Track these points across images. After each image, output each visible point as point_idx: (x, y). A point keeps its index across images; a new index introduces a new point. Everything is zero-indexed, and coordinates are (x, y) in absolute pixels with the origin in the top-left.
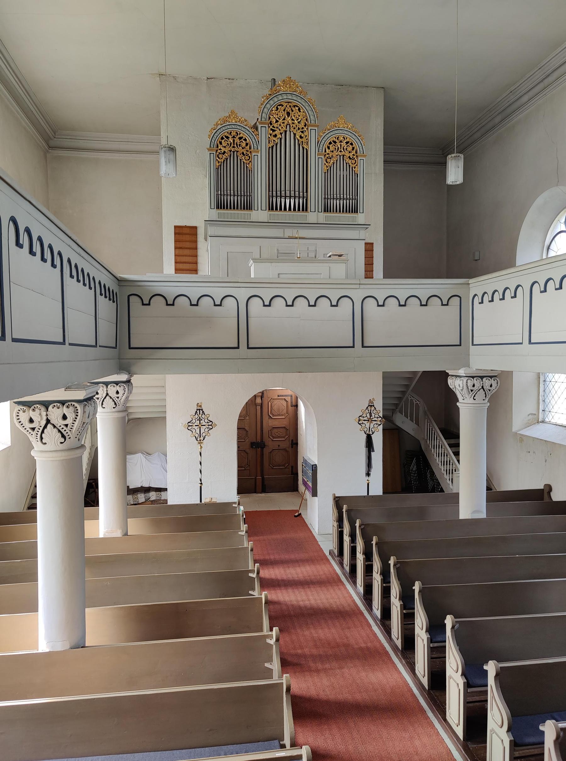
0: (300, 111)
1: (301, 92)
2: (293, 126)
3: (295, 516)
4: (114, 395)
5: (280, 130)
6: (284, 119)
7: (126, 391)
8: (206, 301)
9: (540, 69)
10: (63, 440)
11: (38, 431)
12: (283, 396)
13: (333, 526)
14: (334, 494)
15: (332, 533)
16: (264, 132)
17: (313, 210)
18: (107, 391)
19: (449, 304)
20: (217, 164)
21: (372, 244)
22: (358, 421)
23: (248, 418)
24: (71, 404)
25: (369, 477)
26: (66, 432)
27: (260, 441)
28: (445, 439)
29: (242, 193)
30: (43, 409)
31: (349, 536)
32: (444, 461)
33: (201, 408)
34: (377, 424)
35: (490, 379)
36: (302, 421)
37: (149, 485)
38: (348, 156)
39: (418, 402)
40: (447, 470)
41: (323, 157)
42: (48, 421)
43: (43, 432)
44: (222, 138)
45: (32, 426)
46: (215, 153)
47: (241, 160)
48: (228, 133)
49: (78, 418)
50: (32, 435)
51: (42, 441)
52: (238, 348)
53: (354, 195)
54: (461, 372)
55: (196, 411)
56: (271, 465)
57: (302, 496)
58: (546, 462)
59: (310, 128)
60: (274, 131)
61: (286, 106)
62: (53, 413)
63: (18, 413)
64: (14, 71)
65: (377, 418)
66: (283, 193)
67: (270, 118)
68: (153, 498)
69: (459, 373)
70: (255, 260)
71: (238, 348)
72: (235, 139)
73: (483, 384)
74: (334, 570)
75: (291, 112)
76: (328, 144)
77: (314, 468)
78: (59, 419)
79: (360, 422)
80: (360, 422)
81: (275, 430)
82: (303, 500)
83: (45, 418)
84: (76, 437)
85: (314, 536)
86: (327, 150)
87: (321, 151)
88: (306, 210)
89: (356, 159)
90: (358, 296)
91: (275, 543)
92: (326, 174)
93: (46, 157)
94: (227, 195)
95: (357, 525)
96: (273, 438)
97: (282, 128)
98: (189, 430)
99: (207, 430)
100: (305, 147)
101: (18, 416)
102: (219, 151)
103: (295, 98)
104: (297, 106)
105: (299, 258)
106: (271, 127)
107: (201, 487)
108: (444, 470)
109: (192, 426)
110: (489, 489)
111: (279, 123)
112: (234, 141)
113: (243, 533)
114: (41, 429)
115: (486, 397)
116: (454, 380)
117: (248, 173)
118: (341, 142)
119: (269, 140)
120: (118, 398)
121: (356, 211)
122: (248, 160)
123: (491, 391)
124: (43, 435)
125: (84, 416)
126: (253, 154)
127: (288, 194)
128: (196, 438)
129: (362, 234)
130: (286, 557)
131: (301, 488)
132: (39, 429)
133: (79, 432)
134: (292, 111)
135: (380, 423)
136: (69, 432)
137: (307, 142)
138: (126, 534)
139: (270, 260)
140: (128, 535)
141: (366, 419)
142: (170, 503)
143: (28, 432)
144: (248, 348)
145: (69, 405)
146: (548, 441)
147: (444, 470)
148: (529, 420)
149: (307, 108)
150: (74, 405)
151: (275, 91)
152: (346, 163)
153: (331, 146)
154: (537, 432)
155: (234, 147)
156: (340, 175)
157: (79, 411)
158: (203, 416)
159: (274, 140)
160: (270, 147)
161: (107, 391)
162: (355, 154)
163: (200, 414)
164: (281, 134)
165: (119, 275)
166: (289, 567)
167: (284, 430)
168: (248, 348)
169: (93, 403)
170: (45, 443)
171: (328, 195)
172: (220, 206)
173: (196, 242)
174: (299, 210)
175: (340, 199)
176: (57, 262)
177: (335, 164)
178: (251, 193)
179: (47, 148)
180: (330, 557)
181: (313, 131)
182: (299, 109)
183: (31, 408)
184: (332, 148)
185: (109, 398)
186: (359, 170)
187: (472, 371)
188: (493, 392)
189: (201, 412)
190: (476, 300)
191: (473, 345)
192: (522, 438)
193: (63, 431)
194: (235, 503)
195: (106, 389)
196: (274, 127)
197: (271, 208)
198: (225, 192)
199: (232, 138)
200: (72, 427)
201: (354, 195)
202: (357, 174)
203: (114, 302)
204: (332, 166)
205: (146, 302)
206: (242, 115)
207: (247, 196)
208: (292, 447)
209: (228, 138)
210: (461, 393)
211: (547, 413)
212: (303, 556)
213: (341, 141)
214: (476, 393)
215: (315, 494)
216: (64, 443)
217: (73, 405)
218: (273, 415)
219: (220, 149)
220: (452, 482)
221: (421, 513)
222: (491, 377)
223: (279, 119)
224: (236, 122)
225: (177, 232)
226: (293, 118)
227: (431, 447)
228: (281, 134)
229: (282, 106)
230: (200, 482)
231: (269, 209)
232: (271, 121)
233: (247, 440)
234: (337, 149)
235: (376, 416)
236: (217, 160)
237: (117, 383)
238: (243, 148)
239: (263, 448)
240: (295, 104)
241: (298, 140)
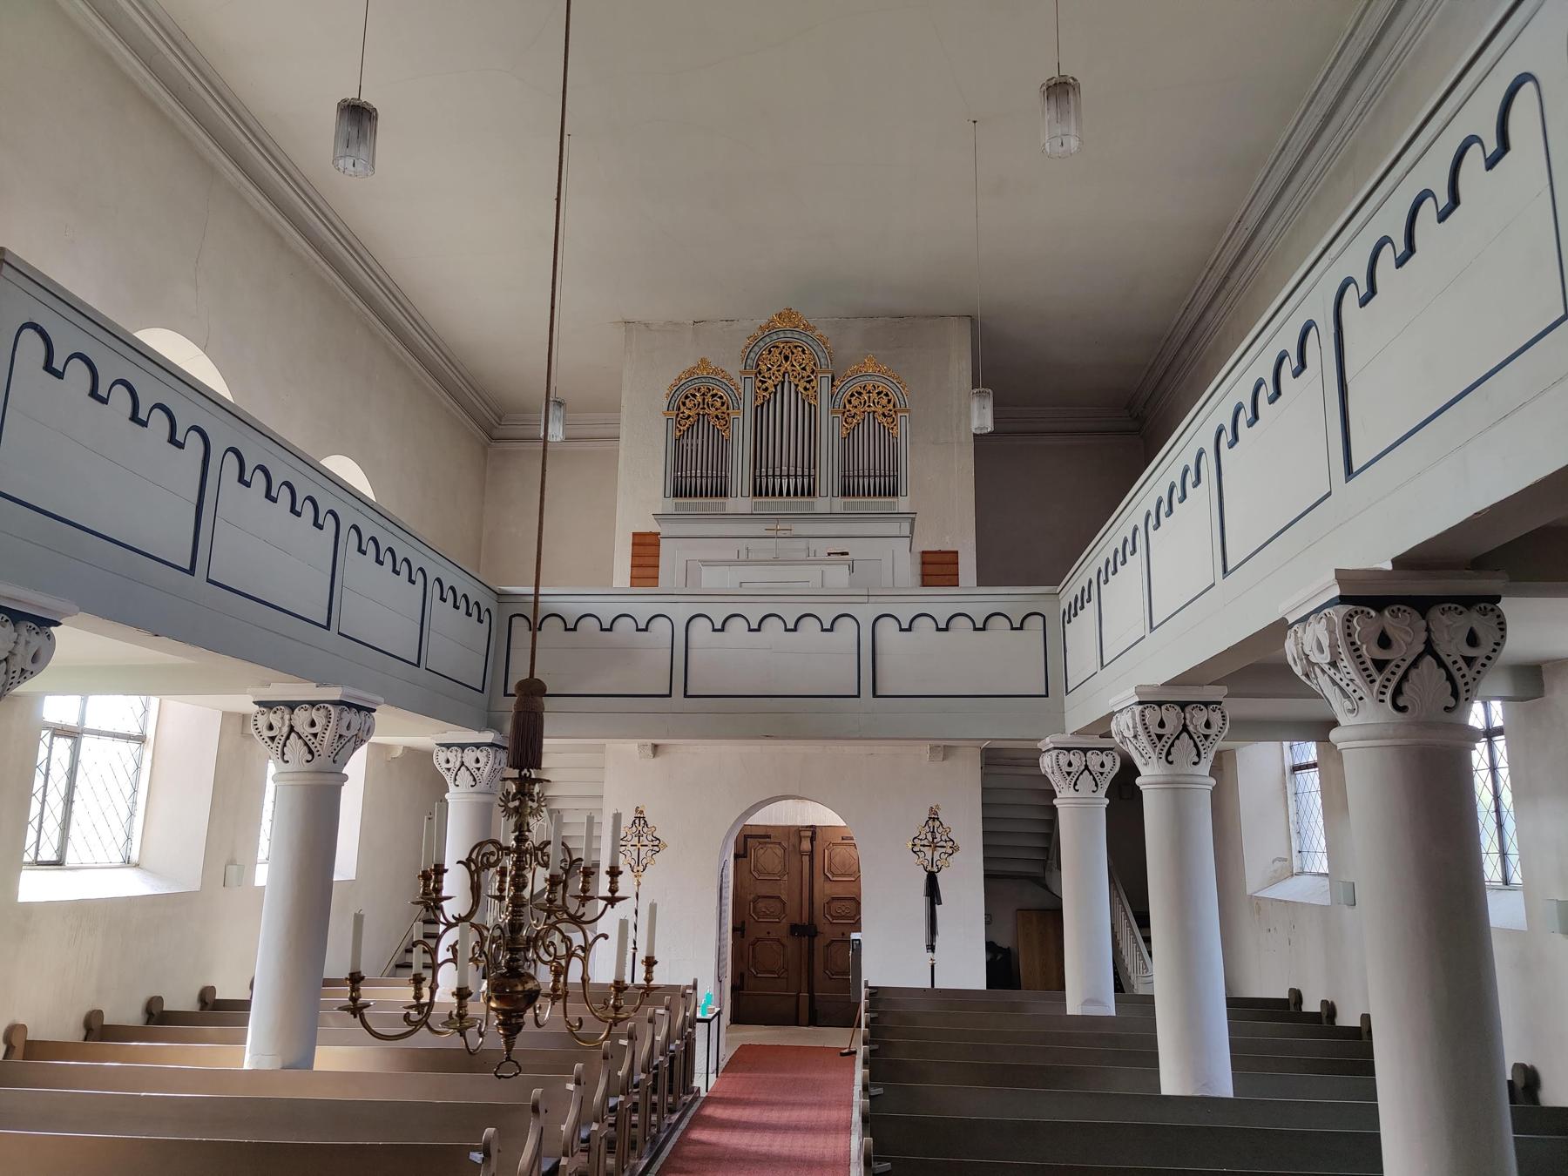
4: (472, 765)
6: (780, 366)
8: (625, 625)
10: (309, 757)
17: (823, 494)
20: (678, 434)
21: (957, 552)
22: (910, 847)
23: (786, 878)
27: (807, 924)
43: (285, 745)
44: (687, 397)
46: (674, 418)
47: (713, 426)
49: (330, 725)
52: (670, 696)
56: (827, 972)
59: (819, 376)
60: (763, 382)
76: (848, 396)
79: (916, 849)
80: (916, 849)
81: (836, 904)
92: (847, 440)
97: (777, 377)
99: (650, 854)
103: (797, 336)
104: (800, 347)
111: (771, 372)
112: (704, 399)
117: (722, 447)
118: (869, 392)
120: (478, 769)
121: (895, 494)
123: (1104, 775)
134: (793, 353)
136: (318, 746)
141: (926, 842)
144: (686, 696)
148: (1275, 871)
149: (815, 348)
152: (879, 424)
155: (704, 408)
158: (645, 829)
159: (764, 396)
160: (757, 406)
168: (686, 696)
170: (288, 762)
174: (803, 494)
184: (855, 402)
189: (642, 822)
197: (758, 492)
218: (833, 875)
223: (773, 366)
225: (636, 541)
226: (794, 363)
228: (775, 386)
229: (777, 347)
233: (784, 921)
237: (478, 746)
238: (883, 407)
240: (797, 344)
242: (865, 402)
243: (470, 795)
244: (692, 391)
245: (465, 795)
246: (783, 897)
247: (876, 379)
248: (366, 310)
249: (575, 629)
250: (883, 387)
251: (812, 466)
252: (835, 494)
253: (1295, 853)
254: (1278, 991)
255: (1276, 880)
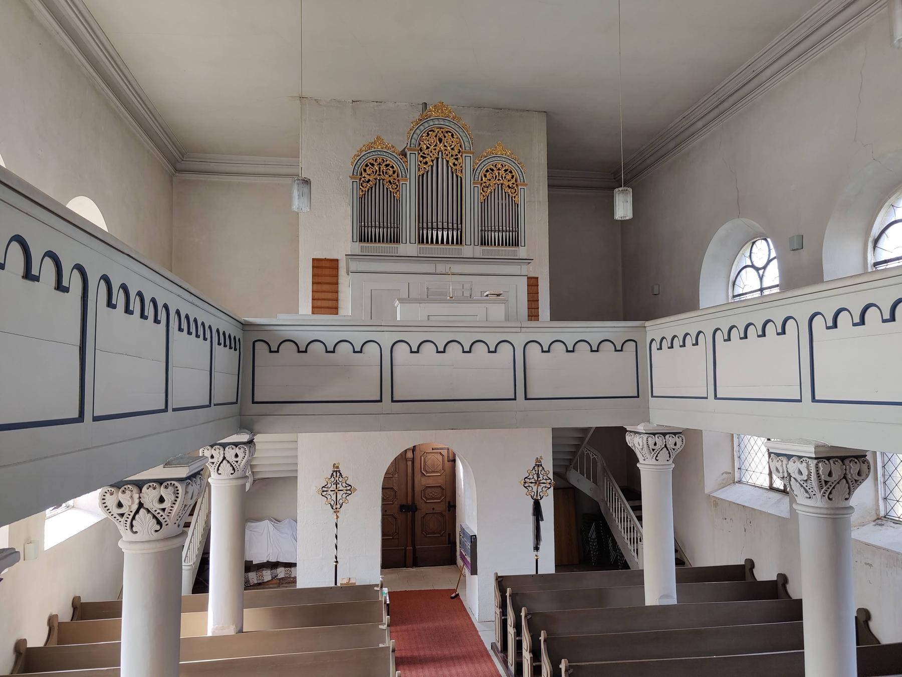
0: (453, 137)
1: (454, 118)
2: (445, 153)
3: (452, 598)
5: (431, 157)
6: (436, 146)
7: (247, 454)
8: (344, 348)
9: (714, 94)
10: (158, 527)
11: (128, 518)
12: (438, 449)
13: (496, 613)
14: (497, 574)
15: (494, 620)
16: (413, 159)
17: (468, 243)
18: (224, 454)
19: (624, 349)
21: (537, 278)
22: (523, 483)
23: (396, 476)
24: (171, 484)
25: (537, 551)
26: (163, 517)
28: (627, 501)
29: (389, 224)
30: (135, 490)
31: (513, 628)
32: (627, 528)
33: (338, 470)
34: (545, 487)
35: (674, 436)
36: (461, 480)
37: (277, 559)
38: (507, 184)
39: (596, 457)
40: (630, 539)
41: (479, 186)
42: (141, 505)
43: (134, 518)
44: (367, 165)
45: (121, 511)
46: (358, 181)
47: (387, 189)
48: (373, 160)
49: (178, 500)
50: (120, 522)
51: (132, 529)
52: (381, 401)
53: (514, 227)
54: (640, 428)
55: (333, 473)
56: (424, 533)
57: (460, 571)
58: (745, 531)
59: (464, 155)
60: (424, 158)
61: (438, 132)
62: (148, 495)
63: (104, 496)
64: (137, 92)
65: (546, 480)
66: (435, 224)
67: (420, 144)
68: (281, 575)
69: (638, 429)
70: (401, 301)
71: (381, 401)
72: (381, 166)
73: (666, 442)
74: (497, 671)
75: (443, 138)
77: (474, 540)
78: (155, 503)
81: (429, 490)
82: (462, 576)
83: (137, 501)
84: (175, 523)
85: (474, 624)
86: (483, 178)
87: (476, 179)
88: (461, 243)
89: (516, 188)
90: (519, 340)
91: (426, 634)
92: (483, 204)
93: (171, 182)
94: (372, 227)
95: (523, 614)
96: (427, 500)
97: (433, 154)
98: (323, 496)
99: (344, 496)
100: (459, 175)
101: (105, 499)
102: (363, 179)
103: (447, 124)
104: (450, 132)
105: (452, 297)
106: (421, 154)
107: (336, 566)
108: (627, 539)
109: (327, 491)
110: (679, 562)
111: (430, 150)
112: (380, 168)
113: (385, 627)
114: (132, 514)
115: (670, 457)
116: (633, 437)
117: (394, 203)
118: (499, 169)
119: (419, 168)
121: (517, 244)
122: (396, 189)
123: (675, 450)
124: (134, 522)
125: (186, 498)
126: (401, 183)
127: (440, 226)
128: (331, 505)
129: (525, 270)
130: (437, 652)
131: (460, 562)
132: (129, 515)
133: (180, 517)
134: (445, 137)
135: (549, 486)
136: (166, 517)
137: (461, 170)
138: (241, 631)
139: (419, 301)
140: (244, 631)
142: (300, 585)
143: (116, 519)
144: (393, 401)
145: (168, 484)
146: (746, 507)
147: (627, 539)
148: (723, 480)
150: (174, 484)
151: (426, 116)
152: (505, 193)
153: (488, 174)
154: (733, 494)
155: (380, 175)
156: (498, 203)
157: (180, 492)
159: (424, 168)
160: (420, 175)
161: (224, 454)
162: (514, 182)
163: (336, 477)
164: (432, 161)
165: (245, 319)
166: (441, 667)
167: (439, 489)
168: (393, 401)
169: (199, 480)
170: (136, 532)
171: (485, 227)
172: (363, 238)
173: (337, 276)
175: (499, 231)
176: (162, 316)
177: (493, 193)
178: (398, 225)
179: (172, 170)
180: (491, 653)
181: (468, 159)
182: (452, 135)
183: (120, 488)
185: (226, 462)
186: (519, 199)
187: (652, 427)
188: (678, 452)
189: (338, 474)
190: (655, 346)
191: (652, 396)
192: (717, 503)
193: (158, 516)
194: (377, 585)
195: (222, 452)
196: (425, 154)
198: (370, 223)
199: (378, 165)
200: (170, 511)
201: (514, 227)
202: (518, 204)
203: (235, 350)
204: (490, 195)
205: (274, 348)
206: (388, 140)
207: (394, 227)
208: (449, 510)
209: (373, 165)
210: (642, 452)
211: (744, 471)
212: (458, 651)
213: (499, 168)
214: (658, 453)
215: (474, 572)
216: (159, 532)
217: (172, 484)
218: (427, 472)
219: (364, 177)
220: (637, 554)
221: (601, 597)
222: (675, 434)
223: (431, 145)
224: (382, 148)
225: (315, 265)
226: (446, 144)
227: (611, 511)
228: (432, 161)
229: (434, 131)
230: (335, 560)
231: (419, 242)
232: (421, 147)
233: (396, 503)
234: (494, 178)
235: (545, 478)
236: (361, 189)
237: (236, 444)
238: (390, 176)
239: (415, 512)
241: (452, 168)
242: (496, 176)
243: (231, 481)
244: (370, 161)
245: (228, 481)
246: (395, 488)
247: (504, 160)
248: (94, 74)
249: (306, 351)
250: (390, 161)
251: (459, 222)
252: (476, 244)
253: (736, 469)
254: (735, 559)
255: (723, 485)
